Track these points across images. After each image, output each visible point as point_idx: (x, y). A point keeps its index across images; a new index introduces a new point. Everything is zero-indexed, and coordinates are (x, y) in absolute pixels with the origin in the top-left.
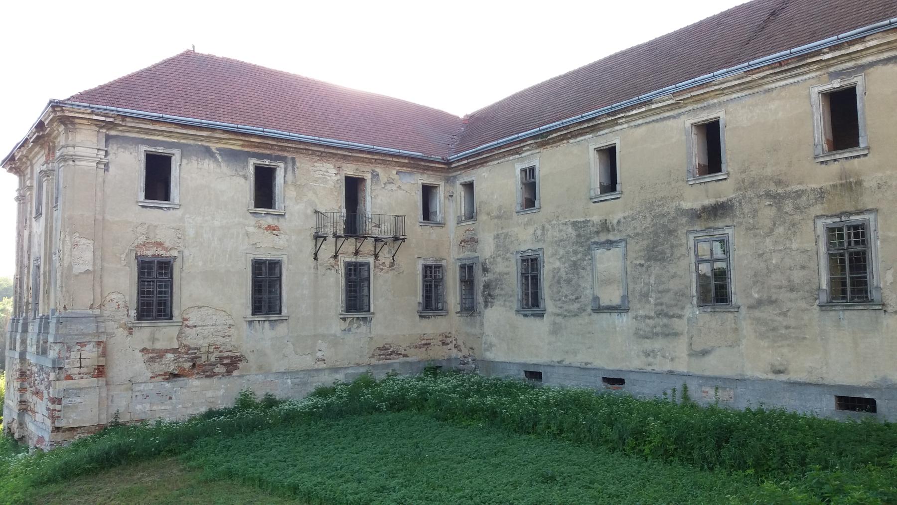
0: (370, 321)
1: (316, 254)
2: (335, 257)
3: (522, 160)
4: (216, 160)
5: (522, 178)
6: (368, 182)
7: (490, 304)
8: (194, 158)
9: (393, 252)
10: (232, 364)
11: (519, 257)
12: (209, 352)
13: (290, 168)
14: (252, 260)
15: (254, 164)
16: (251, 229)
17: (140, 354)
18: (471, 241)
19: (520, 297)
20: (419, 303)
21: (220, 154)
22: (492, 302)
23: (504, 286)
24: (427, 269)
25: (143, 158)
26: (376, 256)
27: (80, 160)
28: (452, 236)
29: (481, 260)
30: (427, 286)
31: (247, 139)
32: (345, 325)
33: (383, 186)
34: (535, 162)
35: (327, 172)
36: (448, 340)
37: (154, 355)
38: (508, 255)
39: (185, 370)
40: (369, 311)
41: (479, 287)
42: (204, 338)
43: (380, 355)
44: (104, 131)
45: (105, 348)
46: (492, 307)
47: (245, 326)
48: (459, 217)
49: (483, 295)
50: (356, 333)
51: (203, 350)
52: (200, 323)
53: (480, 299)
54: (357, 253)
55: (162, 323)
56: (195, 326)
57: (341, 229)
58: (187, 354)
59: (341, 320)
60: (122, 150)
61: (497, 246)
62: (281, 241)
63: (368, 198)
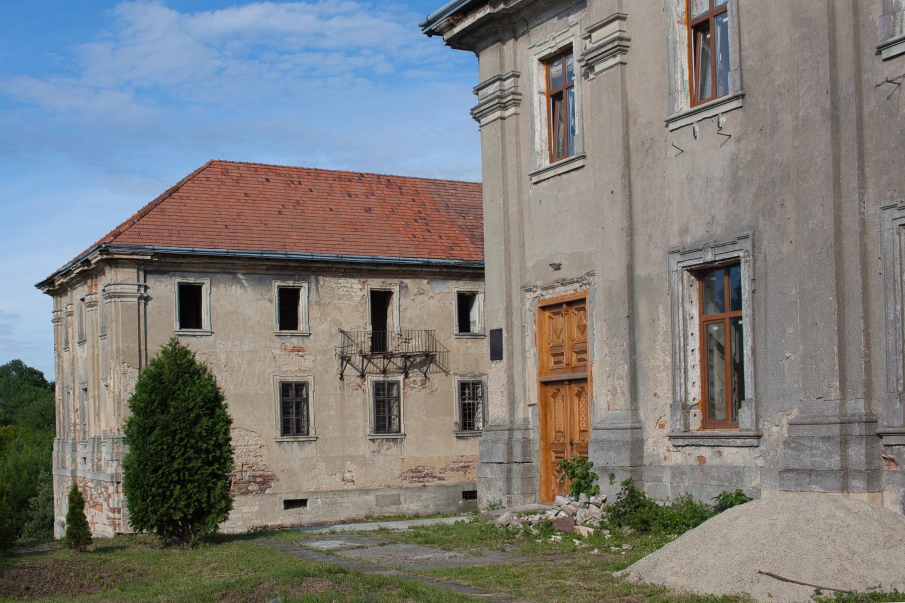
0: (401, 442)
1: (342, 375)
4: (243, 286)
8: (222, 285)
15: (278, 286)
21: (246, 280)
32: (374, 447)
35: (352, 287)
40: (399, 431)
43: (412, 478)
47: (275, 446)
50: (386, 455)
57: (367, 346)
59: (370, 442)
60: (159, 283)
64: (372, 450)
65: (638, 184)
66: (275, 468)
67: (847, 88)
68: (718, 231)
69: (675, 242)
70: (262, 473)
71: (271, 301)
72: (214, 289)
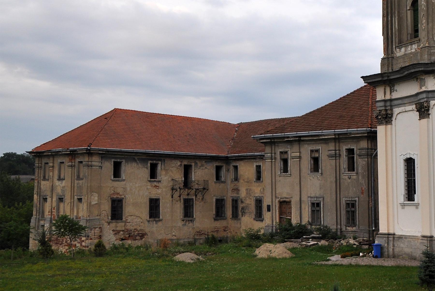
0: (194, 221)
1: (172, 196)
2: (180, 196)
3: (256, 162)
4: (137, 162)
5: (256, 169)
6: (193, 167)
7: (244, 216)
9: (203, 194)
10: (142, 236)
11: (255, 199)
12: (134, 232)
13: (163, 163)
14: (149, 198)
16: (149, 187)
17: (112, 232)
18: (237, 190)
19: (255, 213)
20: (214, 214)
21: (138, 160)
22: (244, 215)
23: (249, 209)
24: (217, 200)
25: (112, 163)
26: (196, 196)
27: (94, 166)
28: (229, 187)
29: (241, 198)
30: (217, 207)
31: (148, 155)
32: (183, 223)
33: (199, 168)
34: (261, 164)
35: (177, 163)
36: (227, 229)
37: (116, 232)
38: (251, 197)
39: (126, 237)
40: (193, 217)
41: (240, 209)
42: (133, 226)
43: (197, 235)
44: (101, 155)
45: (101, 229)
46: (244, 217)
47: (147, 222)
48: (232, 179)
49: (241, 212)
50: (188, 226)
51: (133, 231)
52: (131, 221)
53: (240, 213)
54: (188, 195)
55: (118, 221)
56: (130, 222)
58: (127, 232)
60: (106, 161)
61: (247, 193)
62: (159, 191)
63: (193, 173)
64: (183, 224)
65: (302, 183)
66: (147, 230)
67: (338, 178)
68: (317, 195)
69: (309, 195)
70: (141, 232)
71: (147, 168)
72: (126, 164)
